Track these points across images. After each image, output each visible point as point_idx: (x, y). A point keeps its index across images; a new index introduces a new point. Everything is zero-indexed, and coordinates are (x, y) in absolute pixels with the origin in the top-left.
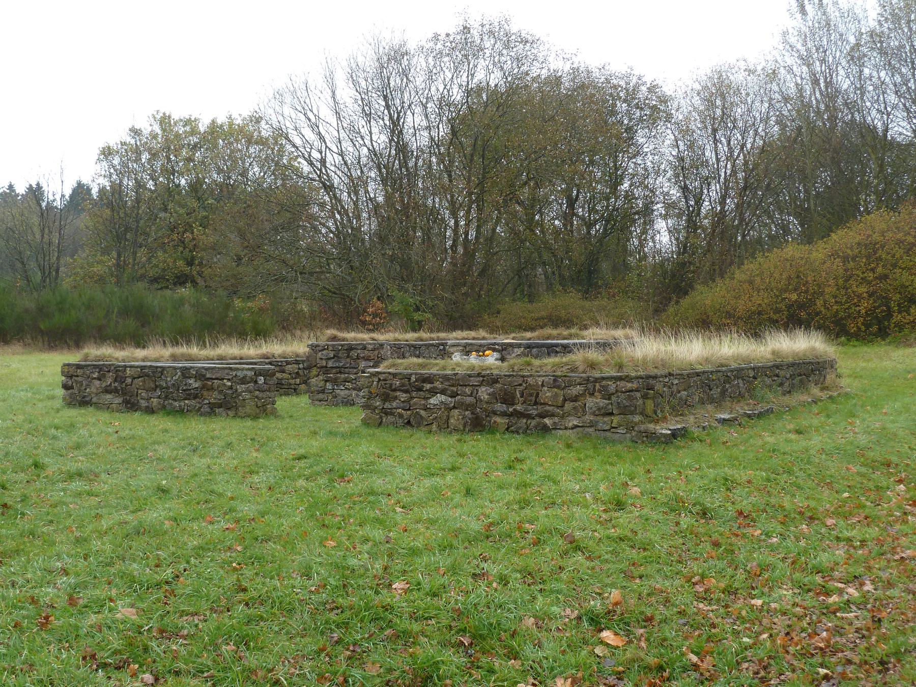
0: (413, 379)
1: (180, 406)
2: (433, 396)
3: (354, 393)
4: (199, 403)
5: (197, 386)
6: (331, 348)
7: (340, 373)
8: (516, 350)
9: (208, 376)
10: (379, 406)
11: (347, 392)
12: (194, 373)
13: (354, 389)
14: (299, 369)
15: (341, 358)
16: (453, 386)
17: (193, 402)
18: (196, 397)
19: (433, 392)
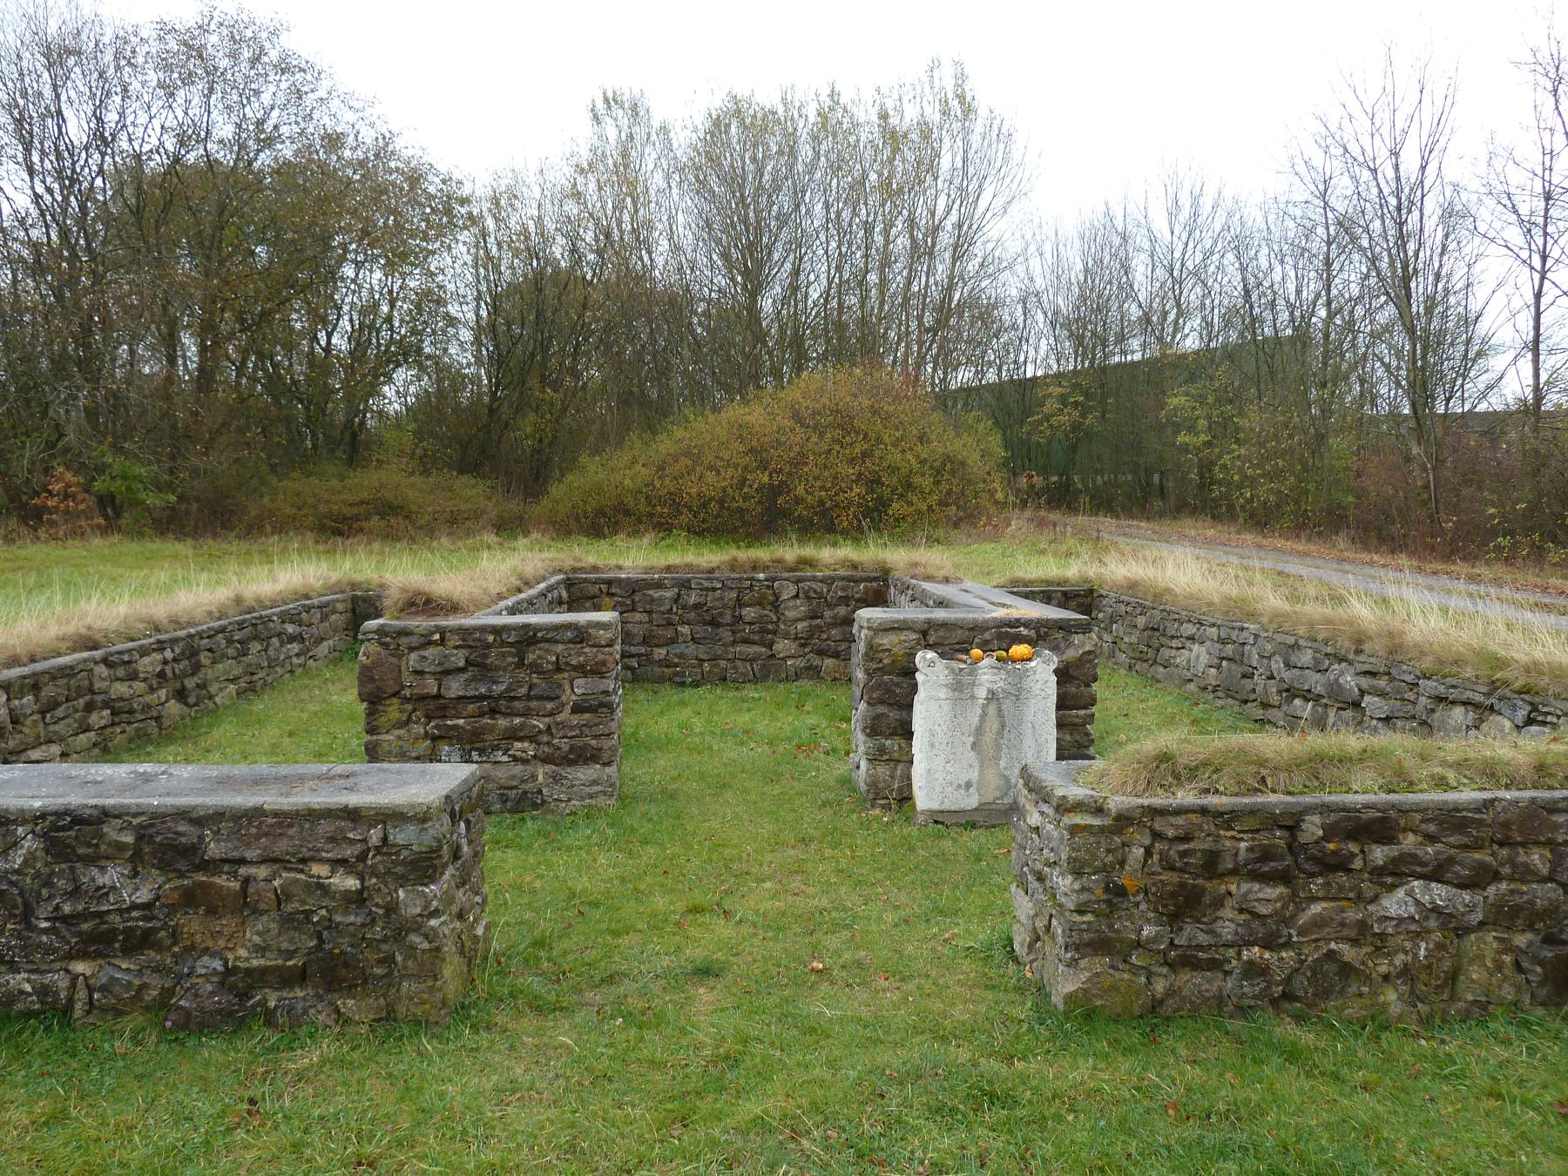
0: (1312, 828)
1: (43, 991)
2: (1392, 888)
3: (542, 772)
4: (158, 969)
5: (143, 896)
6: (454, 640)
7: (493, 712)
8: (1076, 639)
9: (214, 849)
10: (1156, 939)
11: (518, 769)
12: (129, 839)
13: (546, 760)
14: (165, 662)
15: (497, 669)
16: (1476, 846)
17: (123, 969)
18: (137, 942)
19: (1396, 873)
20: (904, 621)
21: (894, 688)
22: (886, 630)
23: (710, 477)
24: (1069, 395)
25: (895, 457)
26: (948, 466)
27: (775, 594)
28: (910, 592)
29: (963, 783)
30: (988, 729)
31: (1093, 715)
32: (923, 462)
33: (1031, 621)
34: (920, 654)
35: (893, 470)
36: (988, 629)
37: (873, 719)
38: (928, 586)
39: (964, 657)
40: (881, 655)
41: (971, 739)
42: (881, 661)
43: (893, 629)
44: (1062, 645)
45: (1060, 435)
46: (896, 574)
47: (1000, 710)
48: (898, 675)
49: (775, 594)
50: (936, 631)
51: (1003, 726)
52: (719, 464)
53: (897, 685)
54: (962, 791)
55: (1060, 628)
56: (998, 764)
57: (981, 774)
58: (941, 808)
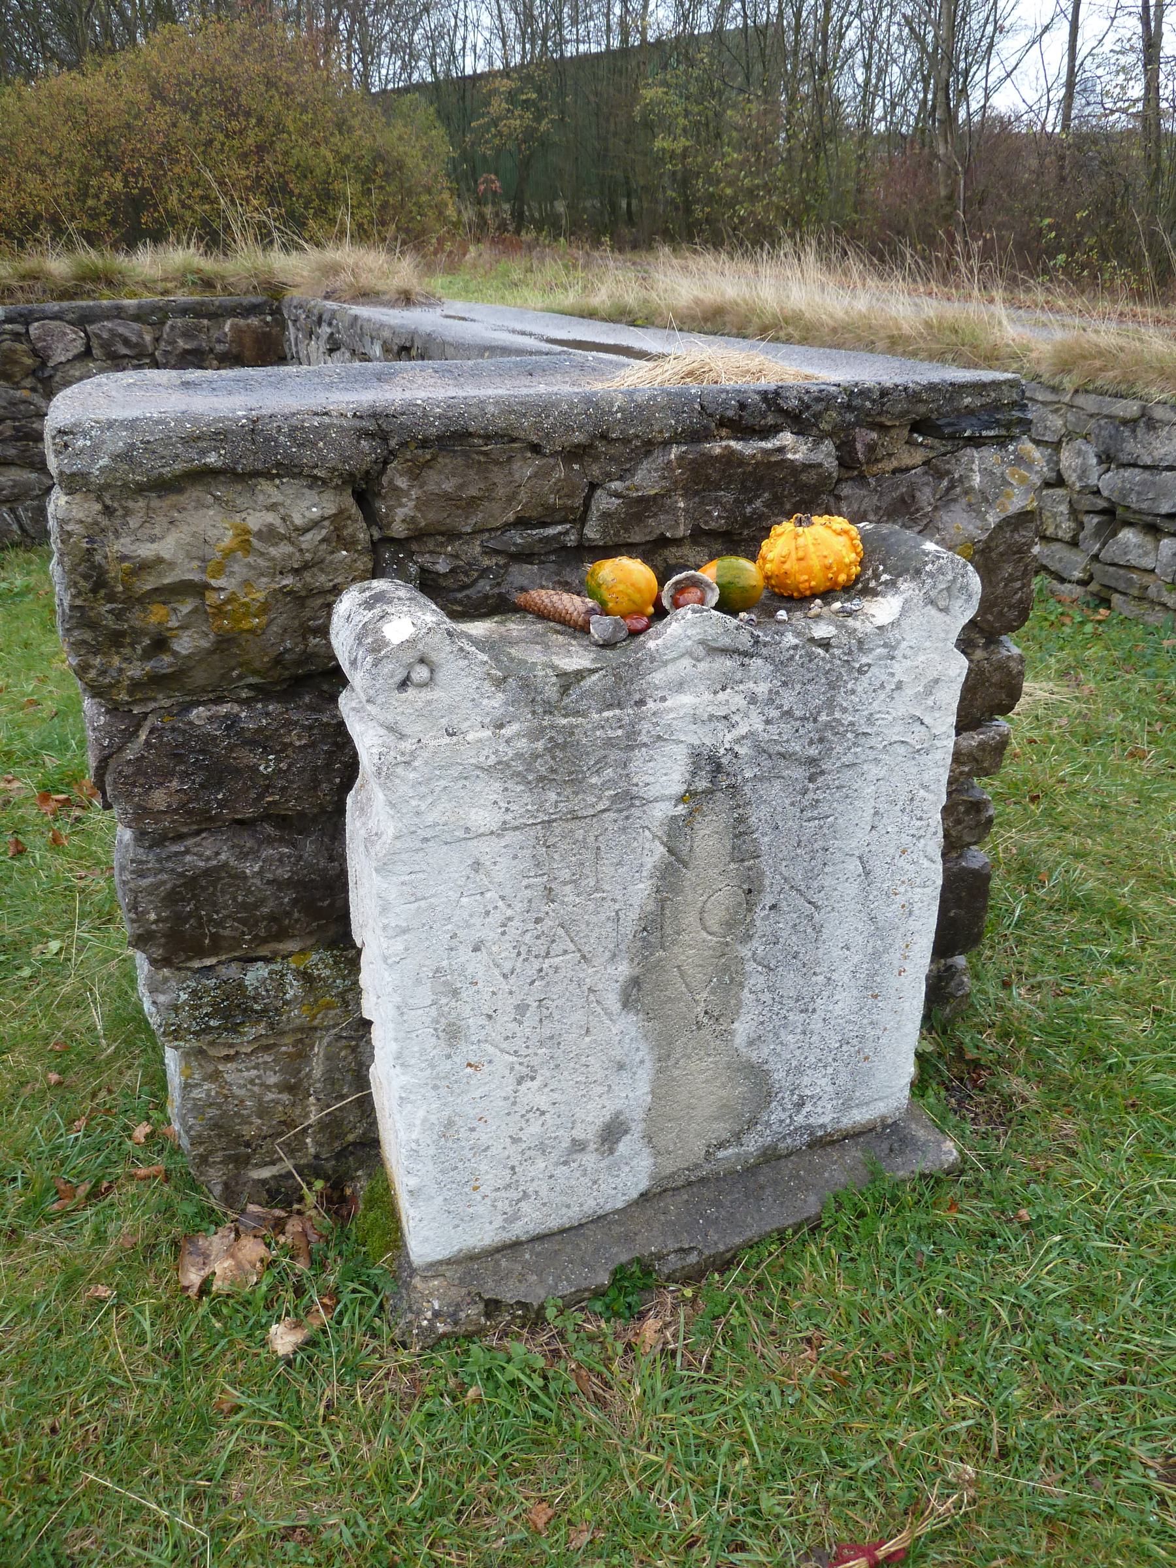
20: (254, 429)
21: (247, 757)
22: (164, 486)
23: (32, 181)
24: (520, 90)
25: (303, 152)
26: (380, 169)
27: (35, 353)
28: (325, 330)
29: (588, 1131)
30: (690, 919)
31: (1004, 743)
32: (344, 160)
33: (824, 398)
34: (347, 603)
35: (305, 172)
36: (649, 447)
37: (172, 898)
38: (364, 311)
39: (572, 604)
40: (157, 615)
41: (624, 969)
42: (160, 644)
43: (203, 475)
44: (925, 497)
45: (510, 145)
46: (294, 295)
47: (740, 830)
48: (263, 693)
49: (35, 353)
50: (416, 472)
51: (751, 892)
52: (44, 160)
53: (261, 741)
54: (589, 1159)
55: (918, 426)
56: (726, 1035)
57: (662, 1088)
58: (508, 1236)
